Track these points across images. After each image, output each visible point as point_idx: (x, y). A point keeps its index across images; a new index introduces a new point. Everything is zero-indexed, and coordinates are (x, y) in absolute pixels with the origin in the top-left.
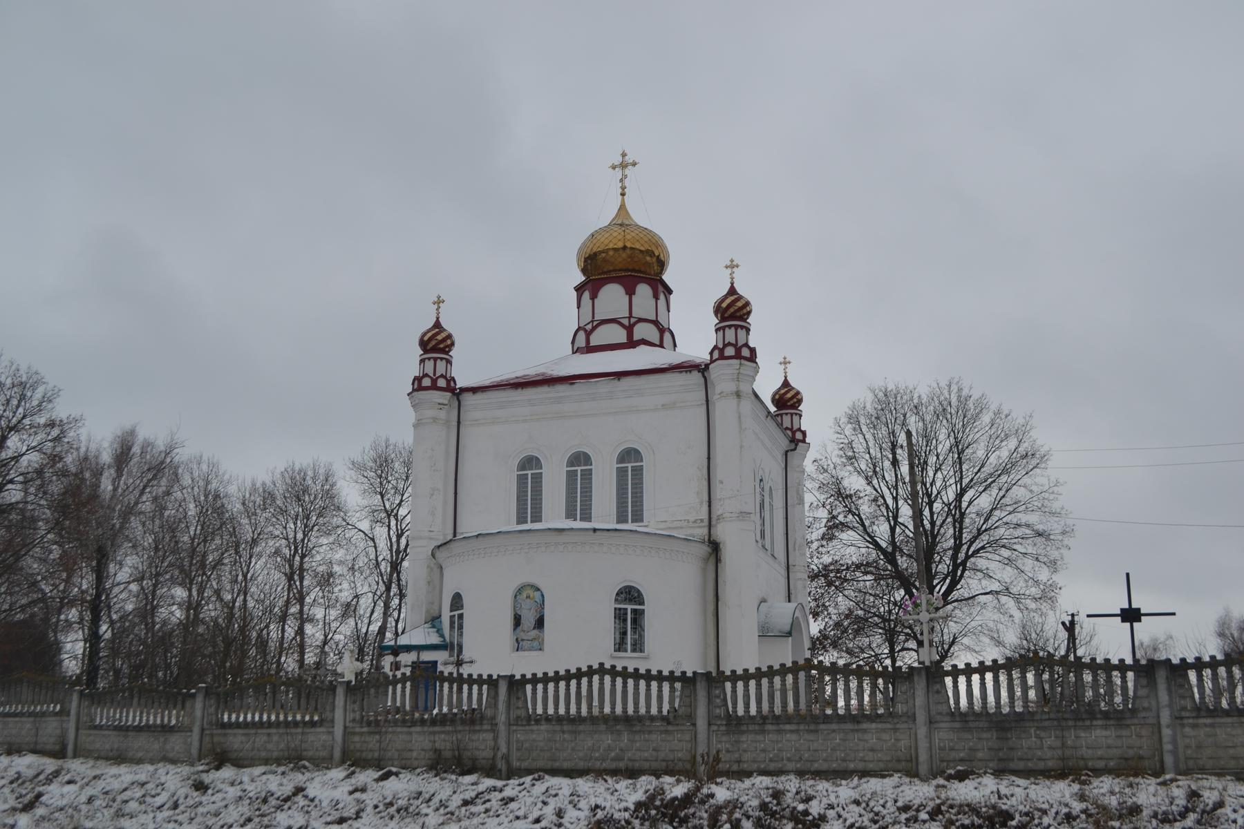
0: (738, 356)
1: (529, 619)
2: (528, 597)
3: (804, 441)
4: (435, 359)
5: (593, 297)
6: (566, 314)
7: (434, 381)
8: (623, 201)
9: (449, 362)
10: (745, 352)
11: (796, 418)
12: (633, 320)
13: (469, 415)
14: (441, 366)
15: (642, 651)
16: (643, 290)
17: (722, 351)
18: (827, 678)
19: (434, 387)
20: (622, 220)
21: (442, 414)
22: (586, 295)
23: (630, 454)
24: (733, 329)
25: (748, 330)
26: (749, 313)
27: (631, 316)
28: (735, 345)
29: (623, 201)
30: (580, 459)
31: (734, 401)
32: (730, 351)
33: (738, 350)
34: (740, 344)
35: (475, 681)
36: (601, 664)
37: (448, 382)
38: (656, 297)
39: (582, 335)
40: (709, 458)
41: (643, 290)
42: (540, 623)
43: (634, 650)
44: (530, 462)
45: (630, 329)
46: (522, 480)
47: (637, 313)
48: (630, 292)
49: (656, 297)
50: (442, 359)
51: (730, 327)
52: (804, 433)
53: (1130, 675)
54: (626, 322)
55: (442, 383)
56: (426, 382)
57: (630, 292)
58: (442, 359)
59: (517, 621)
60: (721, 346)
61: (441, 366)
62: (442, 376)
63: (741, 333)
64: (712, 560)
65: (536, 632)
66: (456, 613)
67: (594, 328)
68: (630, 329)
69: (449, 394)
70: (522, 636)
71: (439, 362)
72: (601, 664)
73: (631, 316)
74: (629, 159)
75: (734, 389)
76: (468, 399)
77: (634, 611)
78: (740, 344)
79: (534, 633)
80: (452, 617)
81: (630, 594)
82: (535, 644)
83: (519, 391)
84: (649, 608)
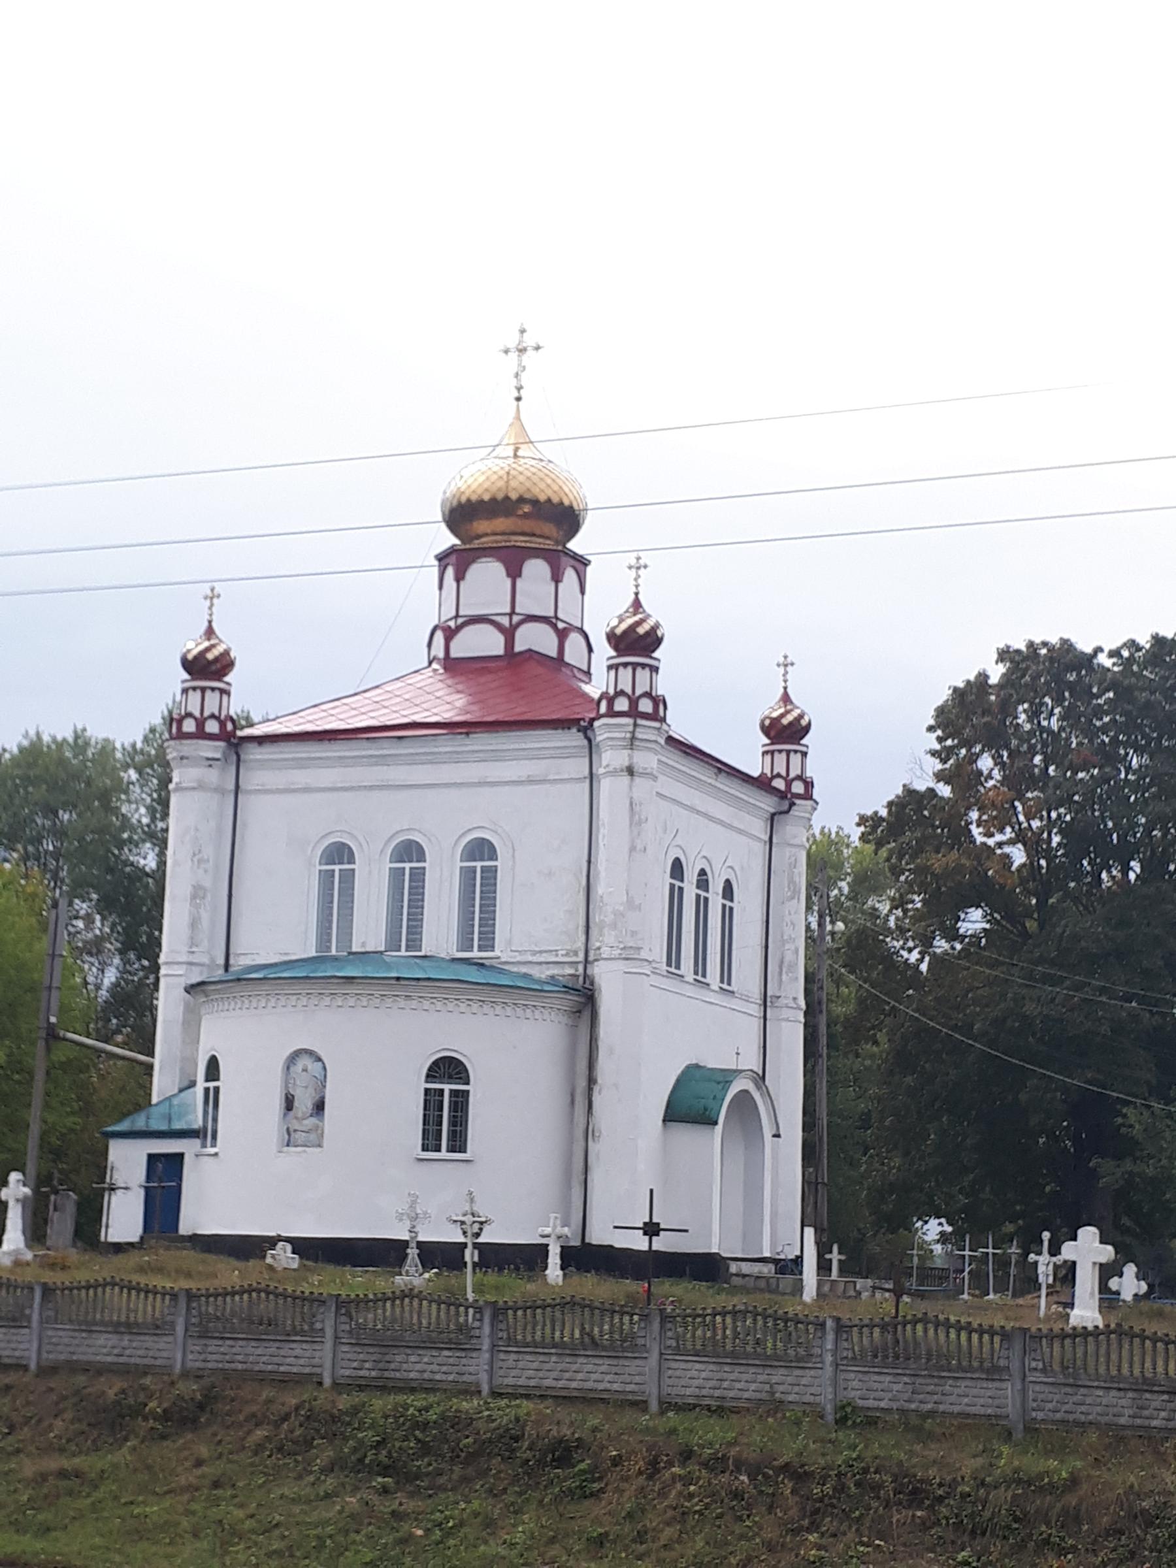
0: (633, 712)
1: (304, 1103)
2: (305, 1070)
3: (808, 796)
5: (459, 578)
6: (417, 598)
10: (646, 706)
11: (795, 759)
12: (516, 619)
13: (253, 779)
14: (212, 700)
15: (463, 1150)
16: (536, 569)
17: (611, 701)
19: (201, 734)
21: (212, 776)
22: (450, 572)
23: (481, 849)
25: (655, 669)
27: (513, 613)
30: (410, 851)
31: (626, 779)
32: (622, 705)
37: (222, 724)
38: (557, 578)
39: (439, 637)
40: (589, 862)
41: (536, 569)
42: (319, 1107)
43: (451, 1150)
44: (340, 853)
45: (509, 634)
46: (326, 878)
47: (525, 606)
48: (514, 573)
49: (557, 578)
51: (625, 665)
52: (809, 785)
54: (505, 621)
55: (212, 727)
56: (189, 726)
57: (514, 573)
59: (289, 1103)
60: (611, 692)
61: (212, 700)
62: (213, 716)
63: (643, 675)
64: (587, 1015)
65: (313, 1120)
66: (211, 1085)
67: (459, 628)
68: (509, 634)
69: (222, 744)
70: (295, 1125)
71: (208, 693)
73: (513, 613)
74: (529, 340)
75: (626, 764)
76: (253, 753)
77: (454, 1093)
79: (312, 1121)
80: (207, 1090)
81: (448, 1068)
82: (313, 1137)
83: (326, 745)
84: (476, 1091)
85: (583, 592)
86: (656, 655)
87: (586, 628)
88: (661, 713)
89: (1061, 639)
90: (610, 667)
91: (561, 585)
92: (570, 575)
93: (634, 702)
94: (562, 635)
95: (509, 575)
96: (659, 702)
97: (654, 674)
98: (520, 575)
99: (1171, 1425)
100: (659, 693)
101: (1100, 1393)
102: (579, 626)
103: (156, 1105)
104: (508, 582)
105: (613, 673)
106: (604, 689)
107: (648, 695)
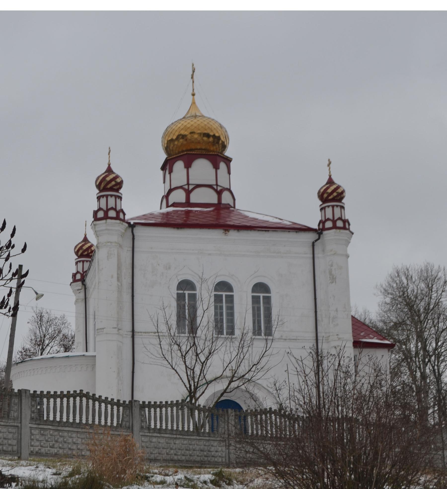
4: (333, 206)
7: (106, 213)
8: (193, 99)
9: (342, 207)
10: (340, 224)
12: (191, 187)
14: (111, 202)
18: (361, 427)
20: (193, 114)
23: (261, 287)
24: (113, 198)
26: (343, 198)
27: (188, 184)
28: (115, 209)
29: (193, 99)
33: (334, 222)
34: (336, 218)
35: (65, 396)
36: (81, 391)
37: (118, 213)
50: (337, 206)
53: (121, 408)
58: (337, 206)
60: (324, 219)
61: (111, 202)
63: (118, 201)
71: (335, 208)
72: (81, 391)
73: (188, 184)
78: (336, 218)
85: (229, 173)
86: (343, 201)
87: (232, 189)
88: (347, 226)
89: (232, 159)
90: (321, 209)
91: (219, 171)
92: (222, 165)
93: (334, 222)
94: (219, 193)
95: (185, 167)
96: (346, 222)
97: (343, 210)
98: (219, 168)
99: (1, 420)
100: (346, 218)
101: (230, 425)
102: (229, 187)
103: (228, 392)
104: (185, 170)
105: (323, 211)
106: (320, 219)
107: (340, 219)
